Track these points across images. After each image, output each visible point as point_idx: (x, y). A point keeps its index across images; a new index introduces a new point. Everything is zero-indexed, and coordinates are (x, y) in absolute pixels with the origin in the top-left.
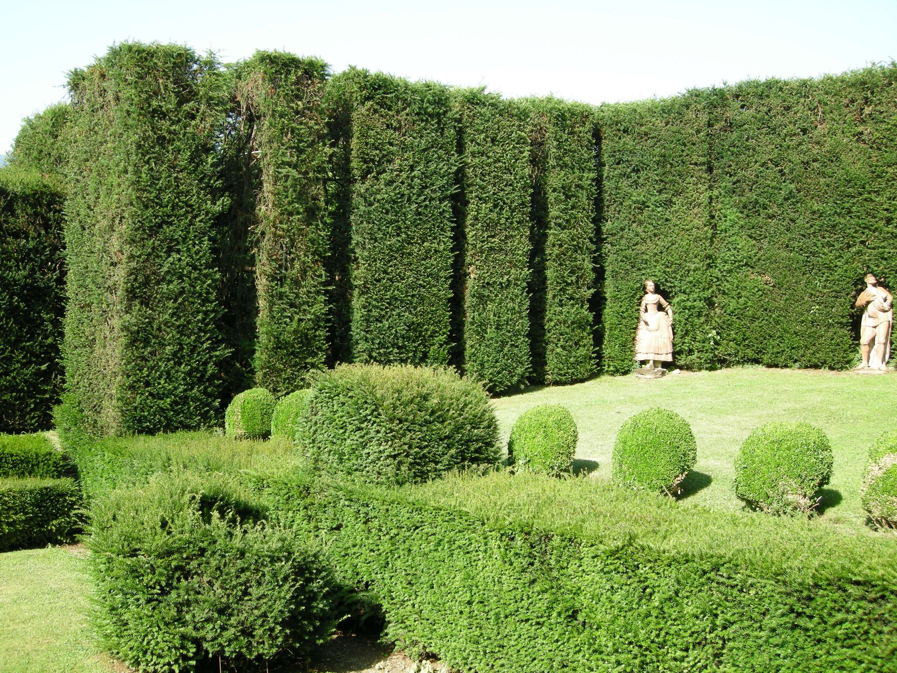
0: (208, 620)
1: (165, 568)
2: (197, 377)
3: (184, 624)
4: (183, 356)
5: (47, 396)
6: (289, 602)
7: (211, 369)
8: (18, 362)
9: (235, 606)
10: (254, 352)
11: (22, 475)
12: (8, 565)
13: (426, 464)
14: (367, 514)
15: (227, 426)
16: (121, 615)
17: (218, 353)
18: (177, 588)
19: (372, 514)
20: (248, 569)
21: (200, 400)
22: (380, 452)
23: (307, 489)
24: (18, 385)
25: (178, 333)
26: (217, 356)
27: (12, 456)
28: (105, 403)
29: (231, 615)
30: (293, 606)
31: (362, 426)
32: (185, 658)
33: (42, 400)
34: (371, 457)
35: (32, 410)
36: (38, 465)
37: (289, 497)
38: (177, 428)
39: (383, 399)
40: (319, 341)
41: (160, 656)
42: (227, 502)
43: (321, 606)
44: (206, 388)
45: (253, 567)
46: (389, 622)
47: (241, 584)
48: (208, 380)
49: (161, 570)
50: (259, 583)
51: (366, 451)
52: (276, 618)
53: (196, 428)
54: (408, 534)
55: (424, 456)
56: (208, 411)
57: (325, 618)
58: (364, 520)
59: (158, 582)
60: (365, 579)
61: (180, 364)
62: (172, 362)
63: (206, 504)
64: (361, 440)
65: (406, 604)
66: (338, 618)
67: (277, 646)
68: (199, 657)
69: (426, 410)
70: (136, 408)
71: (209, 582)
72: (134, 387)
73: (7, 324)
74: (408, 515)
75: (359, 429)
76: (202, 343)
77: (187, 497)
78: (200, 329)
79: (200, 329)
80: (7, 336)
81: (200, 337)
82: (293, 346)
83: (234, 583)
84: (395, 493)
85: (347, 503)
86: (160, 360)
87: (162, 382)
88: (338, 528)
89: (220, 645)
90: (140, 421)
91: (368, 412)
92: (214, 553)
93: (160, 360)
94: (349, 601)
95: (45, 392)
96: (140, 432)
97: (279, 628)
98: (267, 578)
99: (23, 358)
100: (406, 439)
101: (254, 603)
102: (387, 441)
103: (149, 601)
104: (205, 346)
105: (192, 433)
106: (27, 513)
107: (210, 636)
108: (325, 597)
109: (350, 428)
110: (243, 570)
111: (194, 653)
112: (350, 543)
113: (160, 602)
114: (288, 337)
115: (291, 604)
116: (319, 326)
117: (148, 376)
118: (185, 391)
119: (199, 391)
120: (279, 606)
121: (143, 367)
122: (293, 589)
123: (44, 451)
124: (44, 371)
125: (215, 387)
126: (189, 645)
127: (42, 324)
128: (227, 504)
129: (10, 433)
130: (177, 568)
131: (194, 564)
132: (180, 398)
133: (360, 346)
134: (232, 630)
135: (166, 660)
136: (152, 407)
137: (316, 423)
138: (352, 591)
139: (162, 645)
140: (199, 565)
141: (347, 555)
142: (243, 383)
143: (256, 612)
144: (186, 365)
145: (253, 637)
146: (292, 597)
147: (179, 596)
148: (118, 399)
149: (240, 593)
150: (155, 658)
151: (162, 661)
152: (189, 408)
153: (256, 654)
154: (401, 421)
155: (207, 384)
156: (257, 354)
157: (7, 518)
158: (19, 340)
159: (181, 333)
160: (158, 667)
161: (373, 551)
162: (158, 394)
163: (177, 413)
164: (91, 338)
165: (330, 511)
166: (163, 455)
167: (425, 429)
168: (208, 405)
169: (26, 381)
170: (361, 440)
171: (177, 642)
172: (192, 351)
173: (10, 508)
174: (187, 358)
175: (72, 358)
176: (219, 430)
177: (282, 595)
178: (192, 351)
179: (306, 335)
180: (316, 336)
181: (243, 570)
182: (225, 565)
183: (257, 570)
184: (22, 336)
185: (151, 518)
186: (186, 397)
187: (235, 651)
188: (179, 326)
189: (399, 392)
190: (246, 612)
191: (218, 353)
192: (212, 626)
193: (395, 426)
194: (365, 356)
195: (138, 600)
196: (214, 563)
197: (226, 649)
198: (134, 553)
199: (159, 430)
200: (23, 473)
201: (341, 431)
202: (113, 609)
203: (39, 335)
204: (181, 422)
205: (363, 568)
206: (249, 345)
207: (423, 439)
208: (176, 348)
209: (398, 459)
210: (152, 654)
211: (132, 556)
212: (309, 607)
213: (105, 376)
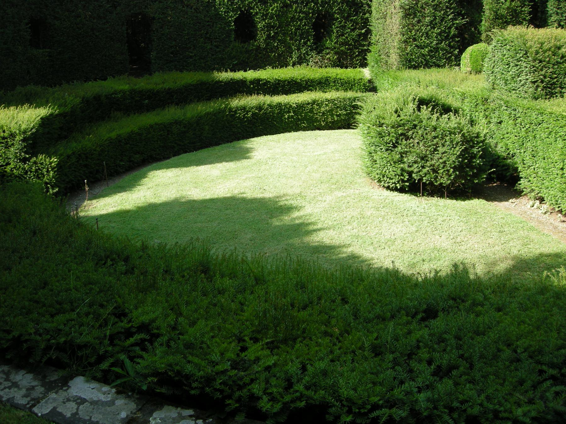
0: (415, 162)
1: (395, 133)
2: (445, 36)
3: (404, 163)
4: (436, 24)
5: (365, 48)
6: (458, 157)
7: (453, 31)
8: (349, 28)
9: (429, 156)
10: (481, 21)
11: (346, 90)
12: (334, 136)
13: (555, 88)
14: (515, 115)
15: (461, 66)
16: (373, 156)
17: (457, 22)
18: (401, 144)
19: (518, 116)
20: (437, 137)
21: (445, 50)
22: (527, 79)
23: (486, 100)
24: (349, 41)
25: (433, 9)
26: (457, 24)
27: (341, 80)
28: (391, 51)
29: (427, 161)
30: (460, 159)
31: (519, 63)
32: (403, 181)
33: (362, 50)
34: (522, 82)
35: (357, 56)
36: (354, 85)
37: (477, 104)
38: (431, 66)
39: (531, 47)
40: (524, 14)
41: (391, 179)
42: (437, 103)
43: (478, 162)
44: (450, 43)
45: (440, 136)
46: (522, 178)
47: (434, 145)
48: (452, 38)
49: (393, 134)
50: (443, 146)
51: (520, 79)
52: (451, 165)
53: (443, 66)
54: (535, 127)
55: (554, 83)
56: (451, 57)
57: (481, 170)
58: (513, 118)
59: (391, 141)
60: (511, 153)
61: (434, 28)
62: (429, 27)
63: (422, 102)
64: (517, 72)
65: (531, 168)
66: (489, 170)
67: (451, 180)
68: (411, 182)
69: (558, 56)
70: (407, 54)
71: (418, 143)
72: (406, 41)
73: (342, 6)
74: (536, 116)
75: (517, 65)
76: (448, 16)
77: (411, 98)
78: (447, 7)
79: (447, 7)
80: (342, 13)
81: (447, 12)
82: (506, 18)
83: (430, 144)
84: (534, 103)
85: (505, 108)
86: (423, 26)
87: (423, 39)
88: (500, 123)
89: (421, 176)
90: (410, 61)
91: (521, 55)
92: (420, 128)
93: (423, 26)
94: (501, 164)
95: (364, 45)
96: (410, 68)
97: (452, 170)
98: (448, 143)
99: (352, 26)
100: (543, 73)
101: (440, 156)
102: (530, 73)
103: (387, 150)
104: (450, 17)
105: (440, 70)
106: (347, 110)
107: (415, 170)
108: (480, 157)
109: (512, 64)
110: (435, 137)
111: (407, 179)
112: (505, 132)
113: (392, 151)
114: (503, 12)
115: (460, 158)
116: (525, 5)
117: (415, 35)
118: (437, 44)
119: (446, 45)
120: (453, 158)
121: (412, 30)
122: (461, 150)
123: (358, 77)
124: (364, 33)
125: (455, 42)
126: (405, 174)
127: (362, 6)
128: (437, 105)
129: (342, 68)
130: (402, 134)
131: (410, 133)
132: (434, 48)
133: (552, 18)
134: (428, 169)
135: (394, 181)
136: (417, 53)
137: (494, 62)
138: (504, 159)
139: (392, 173)
140: (413, 133)
141: (504, 138)
142: (475, 39)
143: (441, 161)
144: (438, 29)
145: (438, 173)
146: (461, 154)
147: (402, 149)
148: (398, 48)
149: (432, 150)
150: (388, 179)
151: (391, 181)
152: (439, 54)
153: (439, 182)
154: (541, 61)
155: (451, 40)
156: (483, 23)
157: (336, 112)
158: (349, 16)
159: (435, 9)
160: (389, 184)
161: (516, 136)
162: (421, 45)
163: (432, 57)
164: (385, 13)
165: (497, 113)
166: (417, 79)
167: (556, 67)
168: (451, 53)
169: (353, 39)
170: (517, 72)
171: (399, 172)
172: (442, 21)
173: (338, 107)
174: (438, 25)
175: (376, 24)
176: (457, 68)
177: (455, 153)
178: (442, 21)
179: (515, 10)
180: (522, 11)
181: (435, 137)
182: (426, 134)
183: (443, 138)
184: (351, 14)
185: (391, 107)
186: (438, 48)
187: (428, 180)
188: (434, 5)
189: (542, 44)
190: (435, 161)
191: (457, 22)
192: (417, 165)
193: (537, 64)
194: (556, 25)
195: (381, 149)
196: (420, 132)
197: (424, 178)
198: (381, 125)
199: (421, 67)
200: (347, 89)
201: (507, 66)
202: (370, 153)
203: (360, 12)
204: (434, 63)
205: (511, 146)
206: (479, 17)
207: (554, 73)
208: (432, 19)
209: (536, 84)
210: (387, 178)
211: (380, 126)
212: (470, 161)
213: (391, 35)
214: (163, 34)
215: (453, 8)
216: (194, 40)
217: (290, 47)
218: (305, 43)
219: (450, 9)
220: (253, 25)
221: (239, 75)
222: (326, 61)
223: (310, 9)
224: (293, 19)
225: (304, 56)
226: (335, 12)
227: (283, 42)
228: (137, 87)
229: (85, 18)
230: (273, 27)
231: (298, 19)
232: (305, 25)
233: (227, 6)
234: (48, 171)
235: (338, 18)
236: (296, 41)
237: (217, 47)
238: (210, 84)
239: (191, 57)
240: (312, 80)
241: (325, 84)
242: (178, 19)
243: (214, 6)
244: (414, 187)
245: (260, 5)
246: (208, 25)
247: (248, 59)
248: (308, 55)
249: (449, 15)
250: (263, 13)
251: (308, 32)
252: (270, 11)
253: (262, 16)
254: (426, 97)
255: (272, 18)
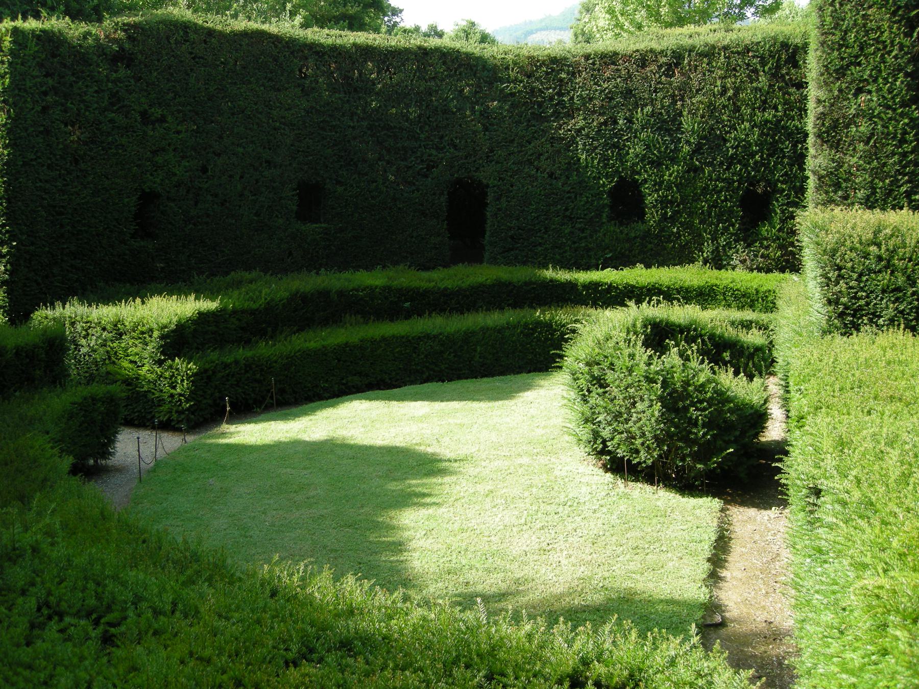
11: (741, 308)
55: (860, 308)
73: (791, 170)
80: (792, 182)
81: (898, 181)
104: (903, 189)
208: (868, 192)
214: (499, 209)
215: (908, 173)
216: (546, 219)
217: (700, 235)
218: (726, 229)
219: (905, 175)
220: (640, 198)
221: (564, 276)
222: (760, 259)
223: (733, 174)
224: (705, 189)
225: (724, 250)
226: (778, 180)
227: (688, 226)
228: (395, 283)
229: (383, 183)
230: (671, 202)
231: (714, 190)
232: (726, 200)
233: (597, 169)
234: (182, 381)
235: (784, 190)
236: (711, 224)
237: (582, 230)
238: (515, 286)
239: (540, 244)
240: (687, 289)
241: (709, 295)
242: (523, 186)
243: (577, 170)
244: (619, 467)
245: (650, 168)
246: (569, 198)
247: (630, 251)
248: (730, 248)
249: (902, 185)
250: (655, 180)
251: (731, 211)
252: (666, 177)
253: (654, 185)
254: (682, 321)
255: (669, 188)
